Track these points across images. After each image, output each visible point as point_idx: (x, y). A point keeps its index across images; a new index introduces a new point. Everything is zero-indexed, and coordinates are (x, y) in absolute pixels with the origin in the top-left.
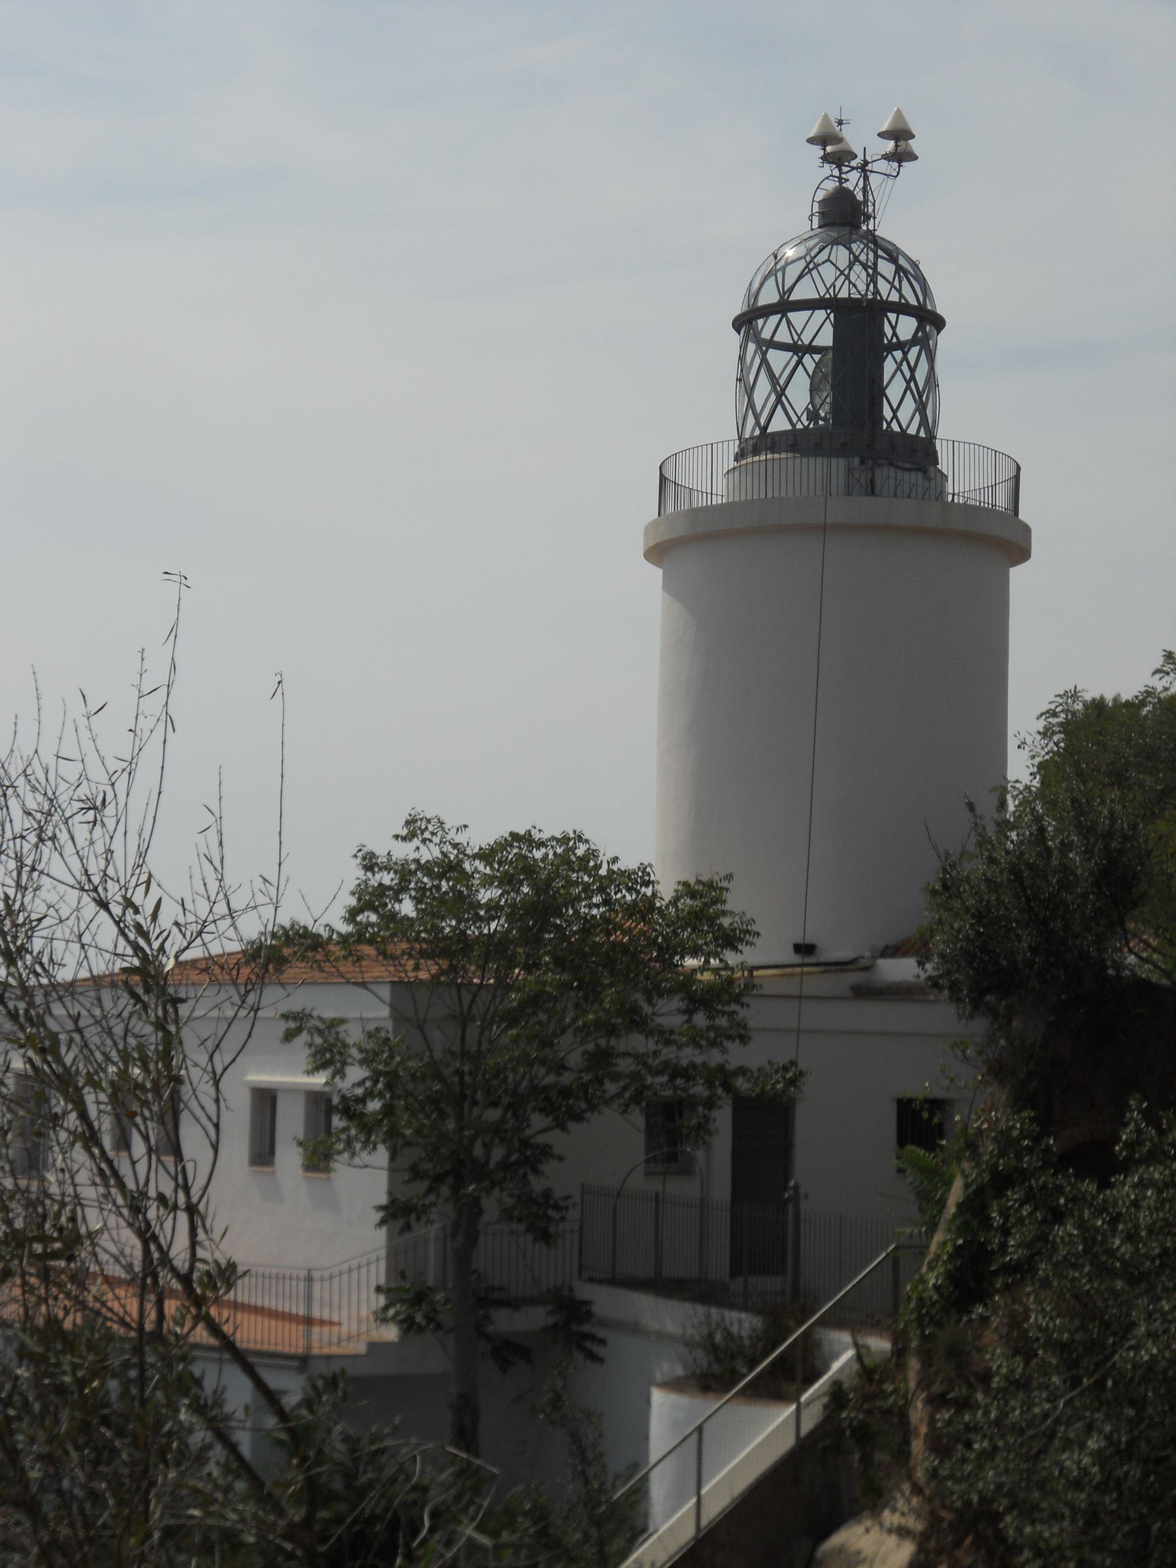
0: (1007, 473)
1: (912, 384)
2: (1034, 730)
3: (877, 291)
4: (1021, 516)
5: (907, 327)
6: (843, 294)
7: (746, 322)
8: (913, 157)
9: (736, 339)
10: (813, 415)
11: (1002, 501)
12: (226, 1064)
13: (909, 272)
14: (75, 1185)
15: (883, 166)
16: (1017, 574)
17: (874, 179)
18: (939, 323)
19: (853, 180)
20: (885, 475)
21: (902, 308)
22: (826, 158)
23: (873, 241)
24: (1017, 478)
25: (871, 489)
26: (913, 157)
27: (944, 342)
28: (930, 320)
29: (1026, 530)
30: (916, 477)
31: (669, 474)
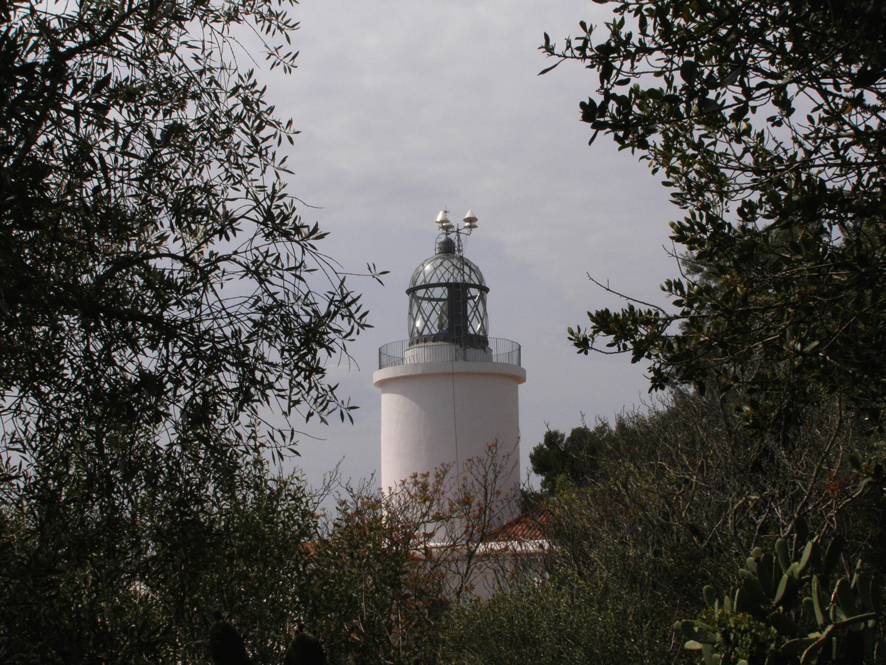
0: (516, 348)
1: (477, 313)
2: (243, 26)
3: (464, 280)
4: (522, 366)
5: (474, 292)
6: (451, 281)
7: (411, 291)
8: (476, 227)
9: (407, 298)
10: (440, 326)
11: (515, 362)
12: (382, 356)
13: (474, 269)
14: (453, 265)
15: (466, 231)
16: (521, 387)
17: (462, 236)
18: (487, 290)
19: (453, 236)
20: (471, 352)
21: (474, 286)
22: (443, 227)
23: (461, 258)
24: (519, 349)
25: (465, 359)
26: (476, 227)
27: (489, 296)
28: (484, 290)
29: (524, 371)
30: (480, 352)
31: (383, 351)
